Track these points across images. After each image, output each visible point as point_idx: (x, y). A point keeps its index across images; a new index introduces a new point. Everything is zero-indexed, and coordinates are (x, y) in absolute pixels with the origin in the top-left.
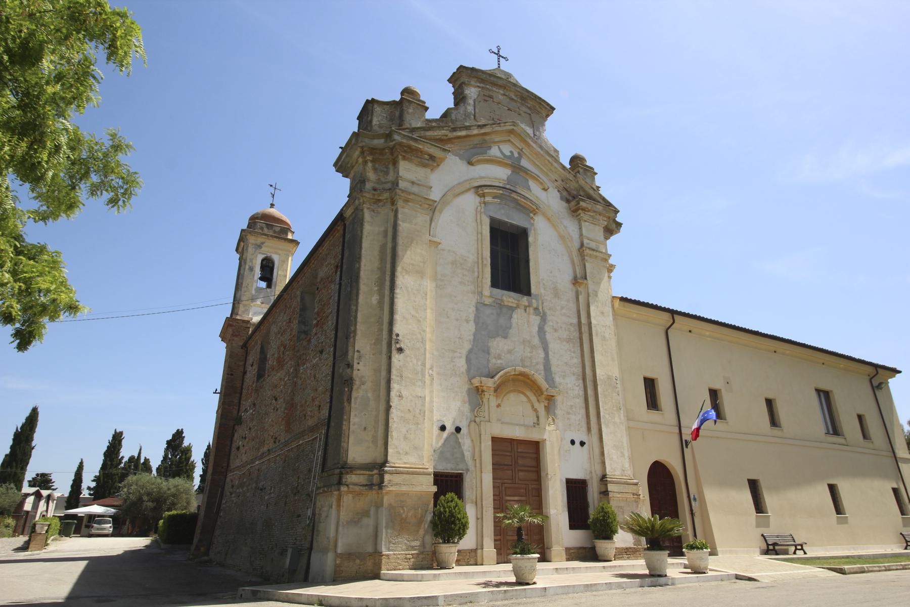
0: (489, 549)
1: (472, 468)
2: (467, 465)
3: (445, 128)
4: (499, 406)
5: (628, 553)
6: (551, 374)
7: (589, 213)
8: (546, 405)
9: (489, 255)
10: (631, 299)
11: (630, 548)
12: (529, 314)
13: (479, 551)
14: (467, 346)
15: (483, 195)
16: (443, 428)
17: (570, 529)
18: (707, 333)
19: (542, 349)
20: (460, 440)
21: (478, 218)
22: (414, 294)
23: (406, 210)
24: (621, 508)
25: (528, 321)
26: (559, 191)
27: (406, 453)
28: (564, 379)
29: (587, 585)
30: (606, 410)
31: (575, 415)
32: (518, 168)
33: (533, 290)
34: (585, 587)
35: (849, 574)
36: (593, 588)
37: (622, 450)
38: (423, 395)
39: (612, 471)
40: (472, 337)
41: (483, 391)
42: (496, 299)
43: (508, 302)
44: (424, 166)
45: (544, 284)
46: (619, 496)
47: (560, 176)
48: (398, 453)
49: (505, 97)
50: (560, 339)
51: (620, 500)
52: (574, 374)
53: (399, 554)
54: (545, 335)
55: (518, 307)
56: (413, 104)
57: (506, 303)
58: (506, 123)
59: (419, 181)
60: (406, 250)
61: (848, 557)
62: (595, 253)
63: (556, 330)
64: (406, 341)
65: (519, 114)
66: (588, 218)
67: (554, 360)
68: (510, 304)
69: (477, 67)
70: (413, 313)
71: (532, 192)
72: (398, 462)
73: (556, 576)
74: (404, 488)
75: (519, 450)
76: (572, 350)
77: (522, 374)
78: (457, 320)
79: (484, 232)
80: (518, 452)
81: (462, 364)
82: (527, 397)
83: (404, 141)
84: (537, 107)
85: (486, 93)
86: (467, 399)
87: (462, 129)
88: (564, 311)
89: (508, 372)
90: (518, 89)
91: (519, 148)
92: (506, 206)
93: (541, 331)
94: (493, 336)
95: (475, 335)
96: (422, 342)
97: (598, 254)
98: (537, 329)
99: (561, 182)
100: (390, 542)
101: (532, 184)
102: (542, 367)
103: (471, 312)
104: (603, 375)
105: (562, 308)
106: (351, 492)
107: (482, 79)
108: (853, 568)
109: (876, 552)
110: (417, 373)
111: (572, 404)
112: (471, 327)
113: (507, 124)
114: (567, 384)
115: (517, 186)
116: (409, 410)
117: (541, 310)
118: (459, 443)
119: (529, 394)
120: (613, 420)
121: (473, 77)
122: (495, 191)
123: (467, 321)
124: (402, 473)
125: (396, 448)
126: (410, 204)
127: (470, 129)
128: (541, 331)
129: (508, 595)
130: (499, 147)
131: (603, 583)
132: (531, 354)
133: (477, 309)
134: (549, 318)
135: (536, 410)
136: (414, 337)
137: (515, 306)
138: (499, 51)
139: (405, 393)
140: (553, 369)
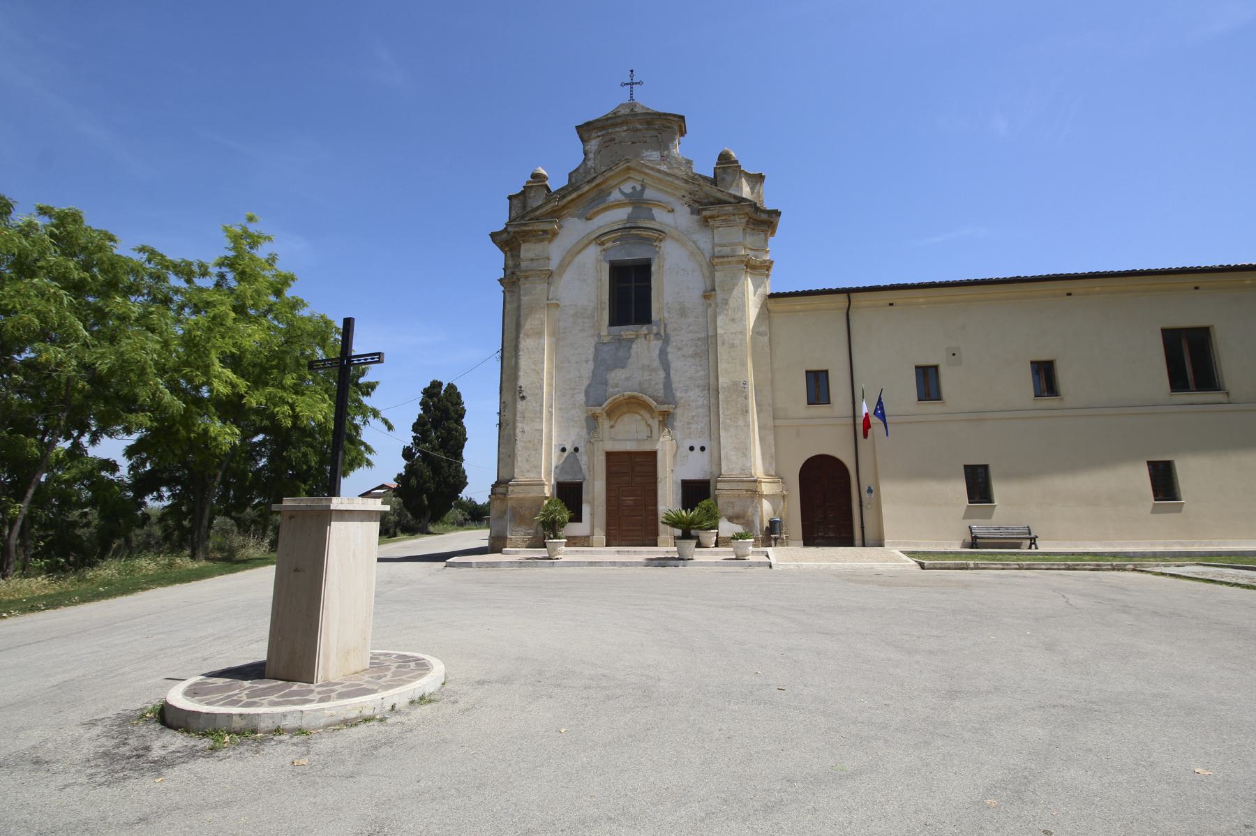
0: (600, 536)
1: (587, 477)
6: (672, 390)
7: (720, 218)
8: (661, 419)
9: (607, 297)
12: (650, 341)
13: (591, 537)
14: (586, 382)
15: (602, 244)
16: (563, 450)
17: (581, 522)
18: (921, 300)
21: (599, 267)
23: (527, 285)
25: (648, 348)
26: (689, 206)
27: (528, 471)
30: (727, 415)
35: (928, 569)
38: (540, 429)
40: (591, 374)
41: (597, 417)
43: (627, 335)
44: (542, 241)
45: (669, 308)
47: (686, 191)
48: (522, 471)
50: (684, 356)
52: (698, 387)
54: (667, 356)
55: (637, 337)
57: (624, 337)
58: (617, 164)
59: (538, 255)
60: (526, 319)
61: (1073, 554)
62: (726, 259)
63: (679, 349)
64: (528, 390)
65: (645, 142)
67: (675, 377)
68: (629, 337)
69: (591, 120)
70: (533, 367)
71: (657, 219)
73: (617, 556)
74: (521, 495)
75: (637, 460)
77: (631, 398)
78: (577, 363)
79: (603, 278)
81: (581, 398)
82: (641, 415)
83: (517, 229)
84: (666, 123)
85: (607, 138)
86: (585, 425)
88: (691, 328)
89: (617, 398)
90: (640, 117)
91: (639, 181)
92: (628, 245)
93: (663, 354)
94: (610, 369)
95: (593, 372)
97: (730, 259)
98: (658, 352)
99: (689, 196)
100: (513, 530)
101: (657, 212)
102: (661, 386)
103: (591, 352)
106: (499, 499)
108: (958, 564)
111: (694, 414)
112: (591, 365)
117: (663, 334)
118: (578, 459)
119: (642, 412)
120: (736, 424)
122: (613, 235)
123: (587, 362)
124: (521, 485)
128: (663, 354)
130: (620, 189)
131: (607, 562)
133: (596, 349)
134: (672, 339)
135: (649, 426)
136: (534, 386)
137: (634, 337)
139: (527, 429)
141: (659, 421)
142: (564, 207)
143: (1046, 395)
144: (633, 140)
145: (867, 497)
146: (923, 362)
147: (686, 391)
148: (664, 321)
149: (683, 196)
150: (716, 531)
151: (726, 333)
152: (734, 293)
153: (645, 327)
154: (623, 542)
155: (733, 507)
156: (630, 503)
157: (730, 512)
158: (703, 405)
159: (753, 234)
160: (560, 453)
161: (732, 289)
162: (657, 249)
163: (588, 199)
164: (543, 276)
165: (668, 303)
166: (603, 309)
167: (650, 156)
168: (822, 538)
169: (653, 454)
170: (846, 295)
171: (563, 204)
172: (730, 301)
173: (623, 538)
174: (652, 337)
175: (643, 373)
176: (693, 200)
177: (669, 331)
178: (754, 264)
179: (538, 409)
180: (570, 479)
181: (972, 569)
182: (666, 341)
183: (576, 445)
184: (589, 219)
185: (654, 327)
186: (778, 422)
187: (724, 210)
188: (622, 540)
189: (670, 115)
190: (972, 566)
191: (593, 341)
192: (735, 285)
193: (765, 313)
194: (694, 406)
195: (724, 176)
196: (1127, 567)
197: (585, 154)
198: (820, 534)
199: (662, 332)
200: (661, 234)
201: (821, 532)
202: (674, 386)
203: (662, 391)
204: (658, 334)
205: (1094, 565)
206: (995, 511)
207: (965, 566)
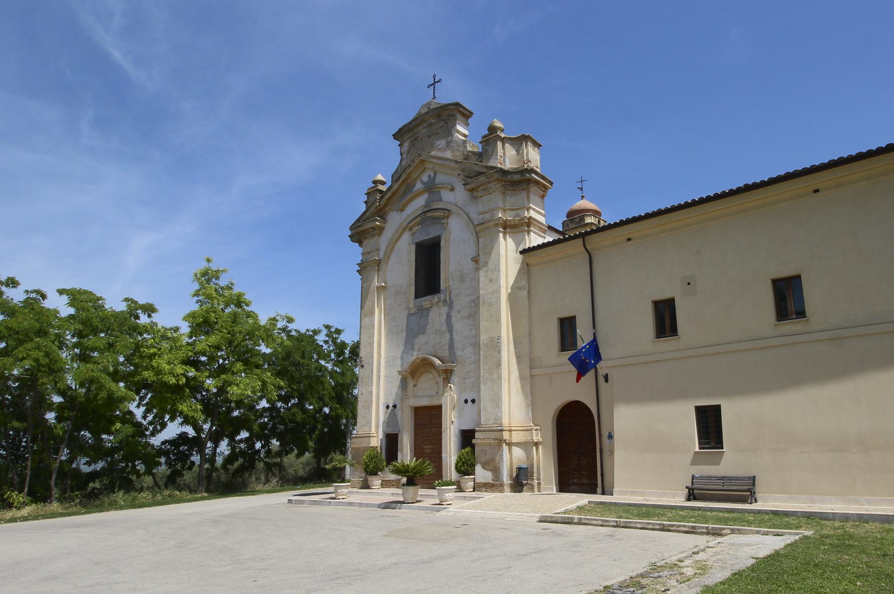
4: (415, 386)
7: (480, 189)
10: (538, 245)
11: (489, 483)
12: (440, 308)
16: (388, 407)
28: (463, 351)
30: (486, 369)
31: (470, 378)
36: (353, 505)
42: (418, 307)
43: (426, 305)
44: (373, 236)
49: (426, 128)
52: (471, 344)
58: (413, 160)
62: (485, 226)
67: (456, 337)
68: (427, 306)
69: (400, 127)
71: (444, 200)
74: (357, 446)
90: (431, 114)
93: (449, 317)
97: (488, 224)
99: (463, 173)
102: (447, 347)
109: (883, 510)
110: (369, 378)
118: (396, 415)
120: (492, 377)
121: (404, 134)
122: (416, 221)
126: (367, 269)
128: (449, 317)
129: (316, 502)
133: (408, 319)
134: (455, 304)
137: (430, 306)
138: (437, 82)
141: (444, 378)
142: (386, 205)
143: (794, 317)
145: (608, 443)
146: (659, 297)
148: (449, 289)
149: (459, 175)
150: (474, 476)
151: (486, 293)
152: (492, 255)
155: (486, 455)
156: (429, 451)
157: (483, 459)
159: (515, 195)
165: (452, 272)
166: (411, 285)
167: (439, 145)
169: (439, 407)
170: (581, 239)
172: (489, 264)
173: (425, 482)
174: (441, 303)
175: (436, 337)
176: (466, 176)
177: (453, 298)
178: (513, 223)
179: (370, 375)
181: (576, 524)
184: (402, 210)
185: (442, 296)
186: (535, 372)
188: (424, 483)
189: (450, 105)
190: (576, 521)
192: (493, 247)
193: (526, 269)
195: (487, 147)
196: (723, 532)
197: (401, 154)
200: (447, 213)
202: (455, 346)
203: (447, 351)
204: (445, 301)
205: (688, 527)
207: (570, 521)
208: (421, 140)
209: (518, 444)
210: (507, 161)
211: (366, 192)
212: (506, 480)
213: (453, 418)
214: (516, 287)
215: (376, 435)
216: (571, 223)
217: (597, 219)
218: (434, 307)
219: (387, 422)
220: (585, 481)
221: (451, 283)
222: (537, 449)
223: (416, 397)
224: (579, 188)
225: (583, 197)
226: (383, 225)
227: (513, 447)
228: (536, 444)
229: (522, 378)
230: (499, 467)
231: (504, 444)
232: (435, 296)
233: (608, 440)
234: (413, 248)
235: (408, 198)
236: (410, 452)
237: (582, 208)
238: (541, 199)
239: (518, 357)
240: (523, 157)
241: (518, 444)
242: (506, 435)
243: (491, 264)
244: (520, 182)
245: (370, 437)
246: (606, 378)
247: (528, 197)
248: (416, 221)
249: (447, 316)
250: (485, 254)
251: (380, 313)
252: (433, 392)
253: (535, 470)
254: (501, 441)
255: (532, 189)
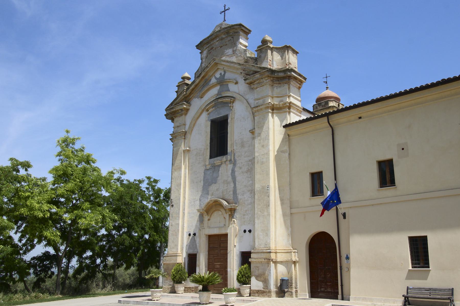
2: (197, 250)
3: (183, 92)
4: (209, 220)
5: (259, 293)
7: (256, 83)
8: (230, 214)
9: (209, 142)
11: (260, 291)
12: (227, 165)
16: (190, 235)
19: (233, 182)
20: (195, 239)
22: (177, 179)
24: (257, 267)
28: (243, 195)
29: (162, 303)
30: (259, 209)
32: (221, 82)
33: (229, 150)
34: (160, 304)
37: (267, 232)
39: (259, 245)
42: (212, 164)
44: (182, 115)
45: (236, 143)
46: (254, 260)
47: (242, 69)
48: (171, 248)
49: (219, 41)
51: (257, 263)
52: (249, 191)
53: (166, 287)
54: (235, 173)
55: (222, 164)
56: (181, 85)
57: (216, 164)
62: (259, 108)
65: (226, 45)
66: (256, 86)
68: (218, 164)
71: (230, 90)
72: (170, 252)
75: (222, 239)
76: (249, 176)
80: (221, 240)
86: (199, 220)
87: (192, 84)
88: (246, 154)
90: (222, 31)
92: (218, 109)
93: (233, 171)
96: (179, 200)
97: (261, 107)
98: (231, 171)
99: (244, 72)
102: (232, 193)
104: (259, 187)
105: (245, 152)
107: (206, 43)
113: (211, 63)
114: (245, 198)
115: (222, 93)
116: (174, 230)
118: (195, 240)
120: (263, 214)
122: (211, 105)
125: (170, 246)
126: (177, 138)
127: (195, 82)
128: (233, 171)
131: (167, 303)
132: (227, 187)
134: (237, 162)
137: (220, 164)
140: (238, 192)
141: (229, 215)
142: (190, 94)
144: (221, 45)
145: (346, 263)
147: (243, 195)
149: (241, 73)
150: (250, 285)
153: (225, 157)
154: (215, 291)
156: (218, 266)
157: (257, 273)
158: (251, 203)
159: (280, 87)
160: (188, 236)
161: (263, 126)
162: (231, 108)
163: (200, 86)
164: (182, 135)
166: (207, 149)
167: (228, 52)
168: (323, 292)
169: (226, 235)
171: (189, 92)
174: (228, 162)
175: (224, 185)
176: (246, 74)
177: (236, 158)
178: (278, 106)
180: (192, 252)
182: (235, 164)
183: (195, 232)
185: (229, 157)
186: (294, 211)
187: (255, 77)
191: (203, 169)
192: (264, 123)
193: (288, 138)
194: (247, 204)
195: (261, 54)
197: (201, 59)
198: (322, 289)
199: (233, 159)
200: (233, 99)
201: (323, 288)
203: (232, 196)
204: (230, 160)
206: (430, 274)
208: (215, 49)
209: (281, 263)
210: (275, 63)
211: (177, 84)
212: (273, 288)
213: (235, 243)
214: (280, 151)
215: (181, 255)
216: (319, 106)
217: (337, 104)
218: (223, 165)
219: (189, 245)
220: (329, 290)
221: (235, 148)
222: (295, 266)
223: (209, 227)
224: (324, 82)
225: (327, 88)
226: (188, 107)
227: (278, 265)
228: (295, 263)
229: (284, 215)
230: (268, 279)
231: (272, 262)
232: (224, 157)
233: (346, 260)
234: (209, 123)
235: (206, 89)
236: (205, 267)
237: (327, 96)
238: (298, 90)
239: (282, 200)
240: (286, 61)
241: (281, 263)
242: (273, 256)
243: (263, 135)
244: (284, 78)
245: (177, 256)
246: (344, 215)
247: (289, 88)
248: (211, 105)
249: (232, 171)
250: (259, 128)
251: (185, 168)
252: (222, 225)
253: (294, 282)
254: (269, 260)
255: (292, 83)
